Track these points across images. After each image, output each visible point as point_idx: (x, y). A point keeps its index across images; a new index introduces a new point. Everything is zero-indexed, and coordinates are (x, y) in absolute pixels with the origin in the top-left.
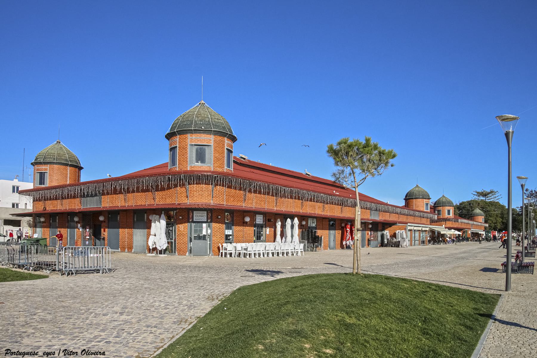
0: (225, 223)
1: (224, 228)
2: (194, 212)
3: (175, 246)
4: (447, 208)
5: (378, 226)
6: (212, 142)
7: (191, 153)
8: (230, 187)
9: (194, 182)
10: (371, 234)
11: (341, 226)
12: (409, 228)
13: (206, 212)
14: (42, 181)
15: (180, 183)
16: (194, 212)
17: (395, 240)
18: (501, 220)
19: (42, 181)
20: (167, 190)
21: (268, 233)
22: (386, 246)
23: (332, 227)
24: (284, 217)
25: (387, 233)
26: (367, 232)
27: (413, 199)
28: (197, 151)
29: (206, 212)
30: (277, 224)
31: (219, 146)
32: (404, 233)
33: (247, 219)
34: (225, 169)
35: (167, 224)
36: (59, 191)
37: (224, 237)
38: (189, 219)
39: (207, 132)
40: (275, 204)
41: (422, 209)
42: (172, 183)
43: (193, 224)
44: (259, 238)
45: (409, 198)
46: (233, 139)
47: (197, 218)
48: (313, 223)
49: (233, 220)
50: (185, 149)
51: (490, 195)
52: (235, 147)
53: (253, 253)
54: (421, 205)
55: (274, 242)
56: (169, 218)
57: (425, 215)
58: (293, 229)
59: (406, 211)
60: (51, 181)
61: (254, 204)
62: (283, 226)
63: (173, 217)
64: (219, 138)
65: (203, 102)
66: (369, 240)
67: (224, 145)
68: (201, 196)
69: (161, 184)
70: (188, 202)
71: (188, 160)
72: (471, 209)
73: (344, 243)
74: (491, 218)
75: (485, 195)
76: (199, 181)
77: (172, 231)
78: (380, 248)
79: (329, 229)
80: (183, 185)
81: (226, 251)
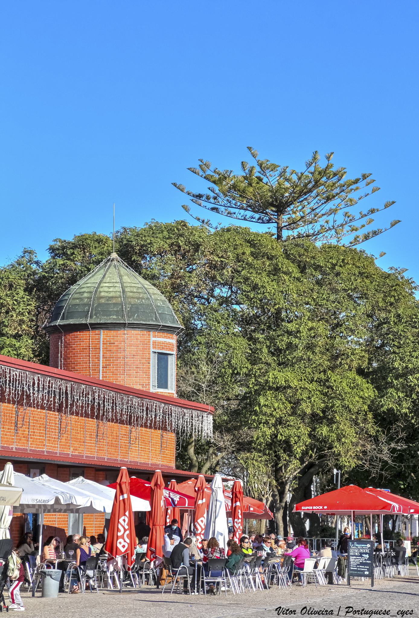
27: (83, 327)
74: (279, 376)
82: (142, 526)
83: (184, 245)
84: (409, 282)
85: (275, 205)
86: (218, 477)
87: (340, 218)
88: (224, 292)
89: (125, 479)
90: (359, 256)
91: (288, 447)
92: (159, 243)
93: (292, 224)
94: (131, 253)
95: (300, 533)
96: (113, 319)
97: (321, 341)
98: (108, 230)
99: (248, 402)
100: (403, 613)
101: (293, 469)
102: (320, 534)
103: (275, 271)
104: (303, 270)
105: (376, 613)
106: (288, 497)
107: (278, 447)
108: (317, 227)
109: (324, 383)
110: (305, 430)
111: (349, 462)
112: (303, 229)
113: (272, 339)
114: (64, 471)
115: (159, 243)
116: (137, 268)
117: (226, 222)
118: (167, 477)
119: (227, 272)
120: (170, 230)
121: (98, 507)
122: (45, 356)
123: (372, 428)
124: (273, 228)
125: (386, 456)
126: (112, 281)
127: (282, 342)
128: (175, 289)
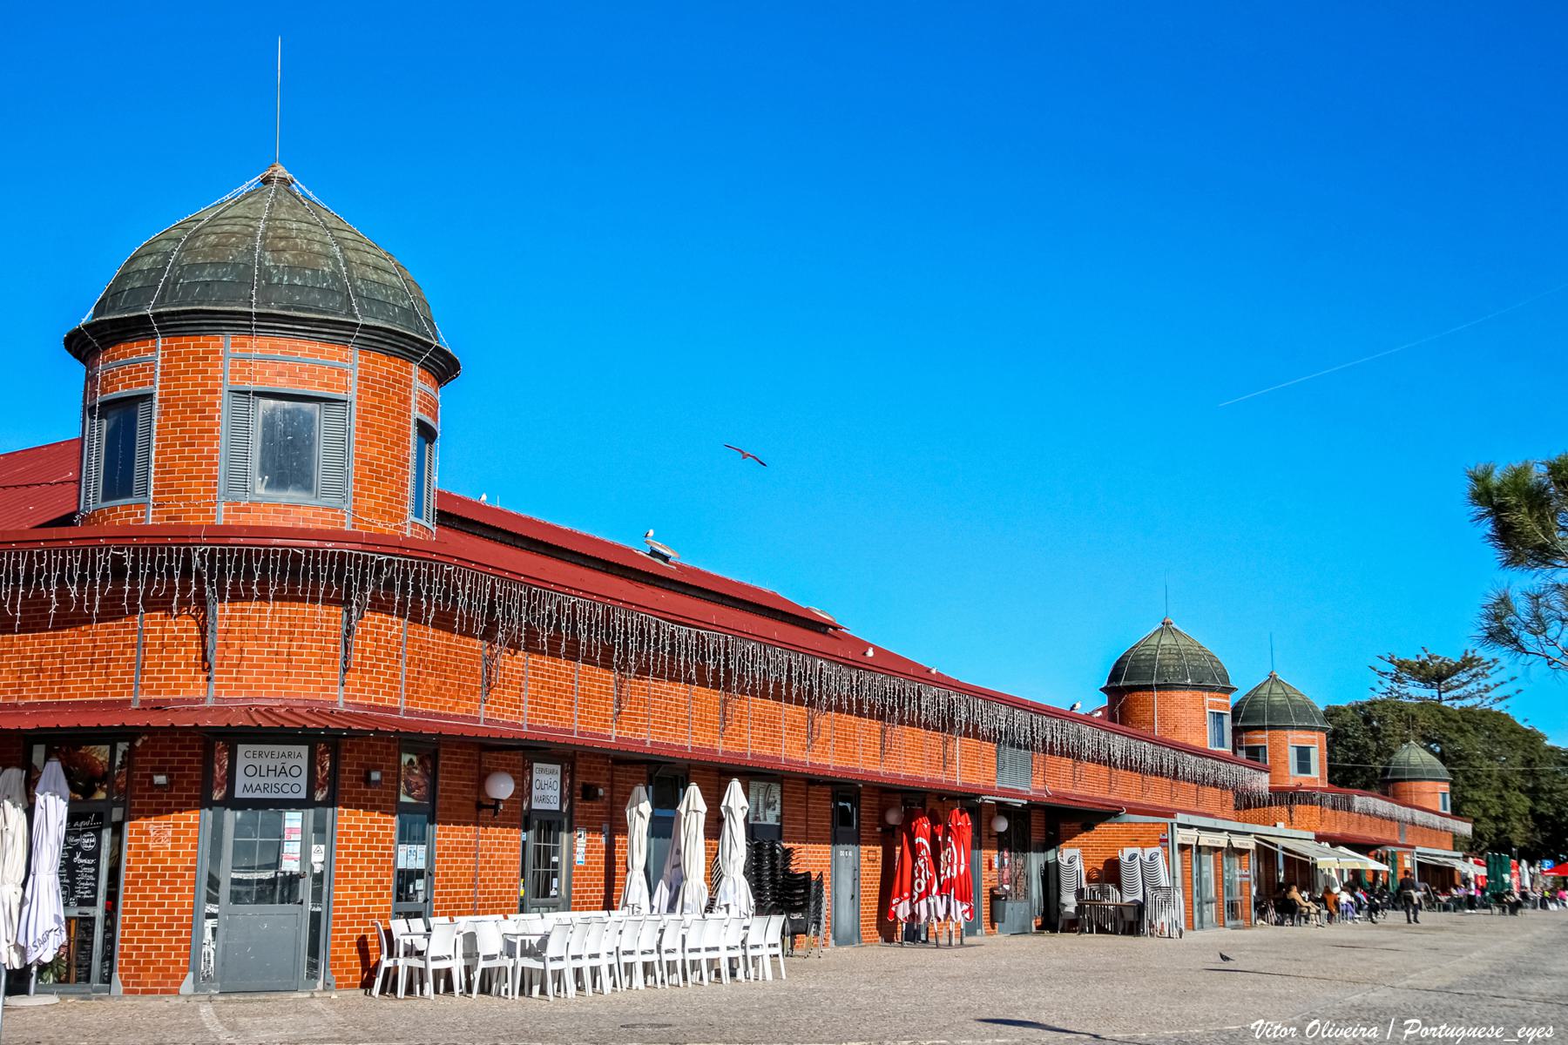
0: (401, 809)
1: (395, 836)
2: (241, 749)
3: (109, 942)
4: (1294, 739)
5: (1029, 823)
6: (353, 381)
7: (237, 438)
8: (444, 622)
9: (263, 584)
10: (1002, 864)
11: (882, 820)
12: (1182, 836)
13: (304, 750)
15: (185, 588)
16: (241, 749)
17: (1114, 898)
18: (1528, 803)
20: (24, 629)
21: (580, 858)
22: (1073, 925)
23: (842, 830)
24: (666, 777)
25: (1074, 858)
26: (985, 853)
27: (1149, 688)
28: (269, 423)
29: (304, 750)
30: (630, 813)
32: (1160, 860)
33: (502, 788)
35: (72, 818)
37: (391, 882)
38: (207, 784)
39: (337, 331)
40: (613, 710)
41: (1194, 741)
42: (134, 591)
43: (231, 817)
44: (541, 889)
45: (1129, 686)
46: (444, 368)
47: (256, 781)
48: (768, 805)
49: (433, 794)
50: (203, 411)
51: (1463, 677)
52: (451, 406)
53: (568, 966)
54: (1193, 719)
55: (609, 905)
56: (81, 783)
58: (715, 841)
59: (1118, 745)
61: (526, 708)
62: (663, 828)
63: (105, 777)
64: (385, 365)
66: (994, 898)
67: (406, 400)
68: (276, 661)
69: (63, 594)
70: (211, 695)
71: (221, 471)
72: (1373, 745)
73: (902, 910)
74: (1477, 794)
75: (1435, 675)
76: (293, 583)
77: (95, 854)
78: (1035, 938)
79: (835, 841)
81: (416, 963)
109: (1500, 797)
123: (1531, 824)
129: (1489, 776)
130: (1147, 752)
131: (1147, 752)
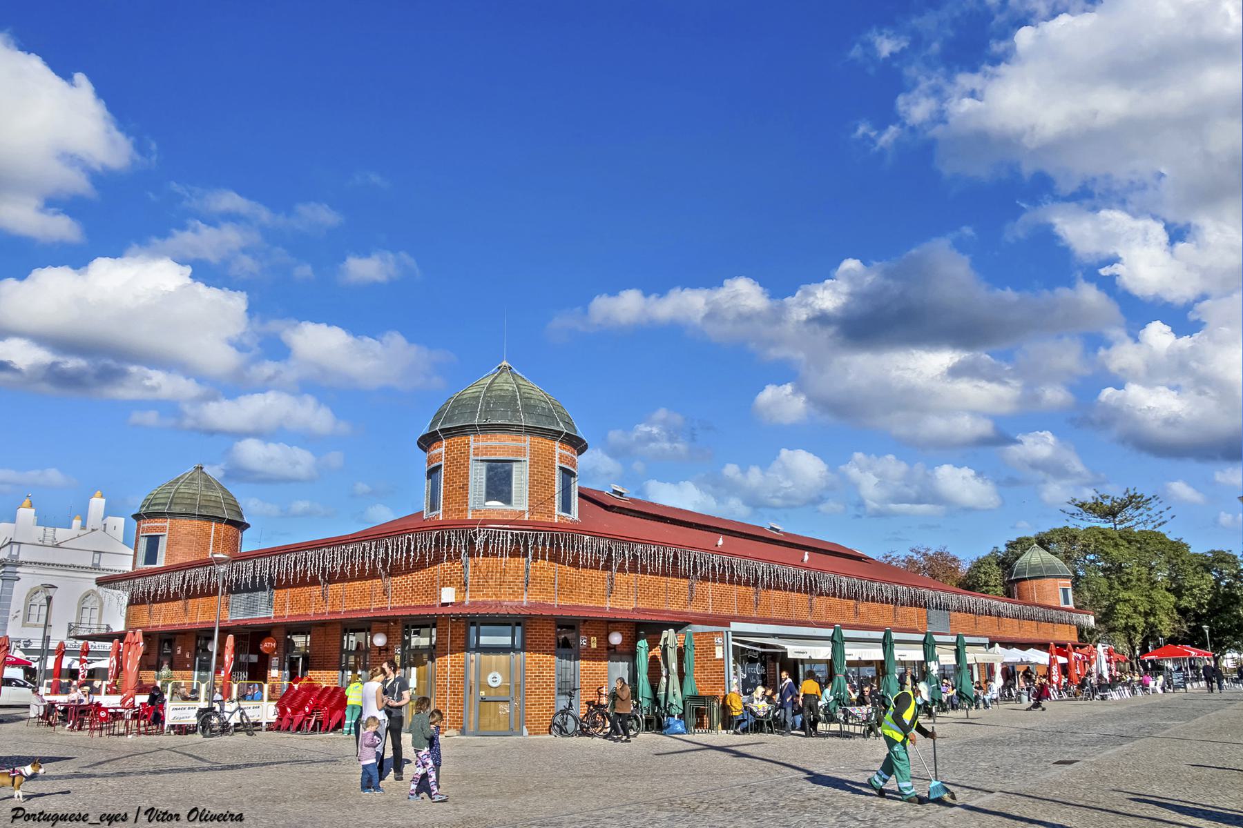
14: (151, 556)
18: (1173, 598)
19: (151, 556)
27: (1025, 579)
31: (540, 464)
34: (558, 515)
36: (201, 575)
46: (578, 445)
57: (1066, 616)
60: (169, 555)
65: (505, 363)
74: (1125, 595)
80: (458, 556)
82: (1065, 669)
83: (1068, 537)
84: (1185, 545)
85: (1111, 513)
86: (1100, 646)
87: (1144, 517)
88: (1092, 557)
89: (1053, 648)
90: (1158, 534)
91: (1134, 628)
92: (1056, 537)
93: (1121, 522)
94: (1043, 542)
95: (1146, 669)
96: (1038, 574)
97: (1144, 576)
98: (1031, 534)
99: (1111, 609)
100: (112, 819)
101: (1138, 639)
102: (1157, 669)
103: (1116, 545)
104: (1129, 542)
105: (64, 818)
106: (1138, 652)
107: (1129, 629)
108: (1134, 522)
109: (1149, 596)
110: (1142, 620)
111: (1167, 634)
112: (1127, 524)
113: (1119, 578)
114: (1024, 646)
115: (1056, 537)
116: (1047, 550)
117: (1088, 525)
118: (1074, 647)
119: (1092, 547)
120: (1061, 530)
121: (1041, 662)
122: (1009, 594)
123: (1177, 616)
124: (1111, 525)
125: (1185, 629)
126: (1036, 556)
127: (1124, 579)
128: (1067, 558)
129: (1139, 580)
130: (1028, 610)
131: (1028, 610)
